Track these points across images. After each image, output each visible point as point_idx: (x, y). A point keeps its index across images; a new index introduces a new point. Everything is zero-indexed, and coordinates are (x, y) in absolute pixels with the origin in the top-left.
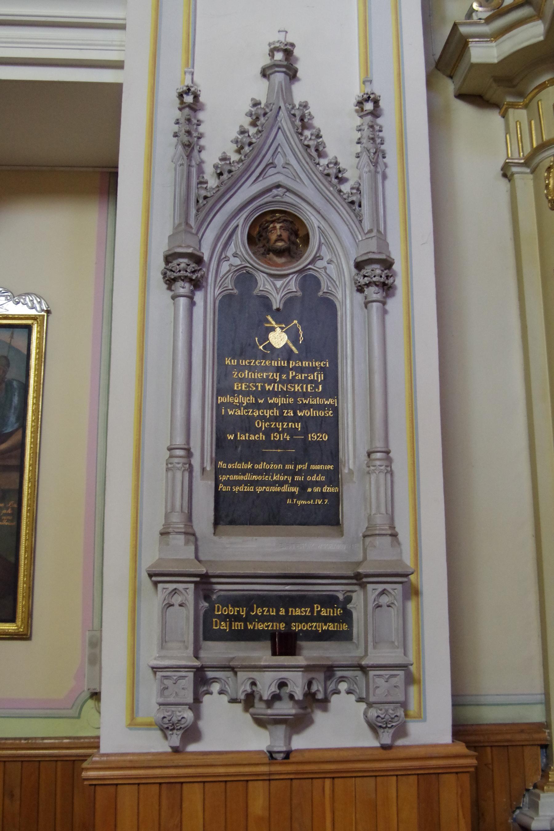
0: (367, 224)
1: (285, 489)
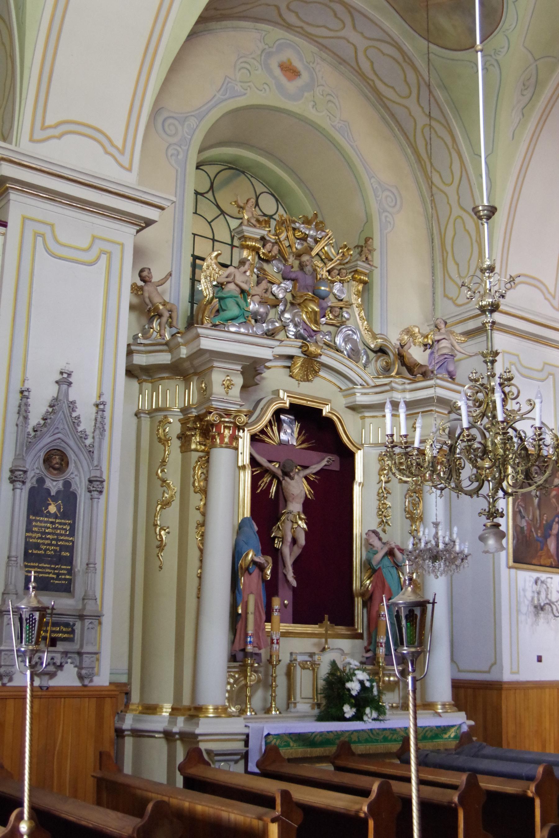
0: (96, 463)
1: (51, 575)
